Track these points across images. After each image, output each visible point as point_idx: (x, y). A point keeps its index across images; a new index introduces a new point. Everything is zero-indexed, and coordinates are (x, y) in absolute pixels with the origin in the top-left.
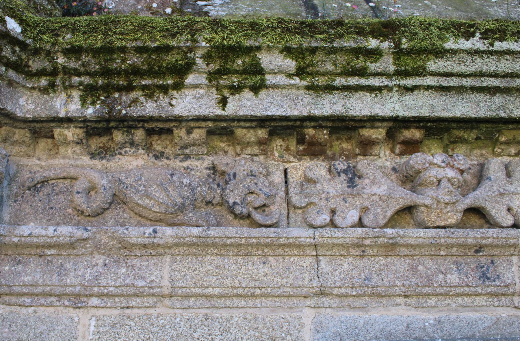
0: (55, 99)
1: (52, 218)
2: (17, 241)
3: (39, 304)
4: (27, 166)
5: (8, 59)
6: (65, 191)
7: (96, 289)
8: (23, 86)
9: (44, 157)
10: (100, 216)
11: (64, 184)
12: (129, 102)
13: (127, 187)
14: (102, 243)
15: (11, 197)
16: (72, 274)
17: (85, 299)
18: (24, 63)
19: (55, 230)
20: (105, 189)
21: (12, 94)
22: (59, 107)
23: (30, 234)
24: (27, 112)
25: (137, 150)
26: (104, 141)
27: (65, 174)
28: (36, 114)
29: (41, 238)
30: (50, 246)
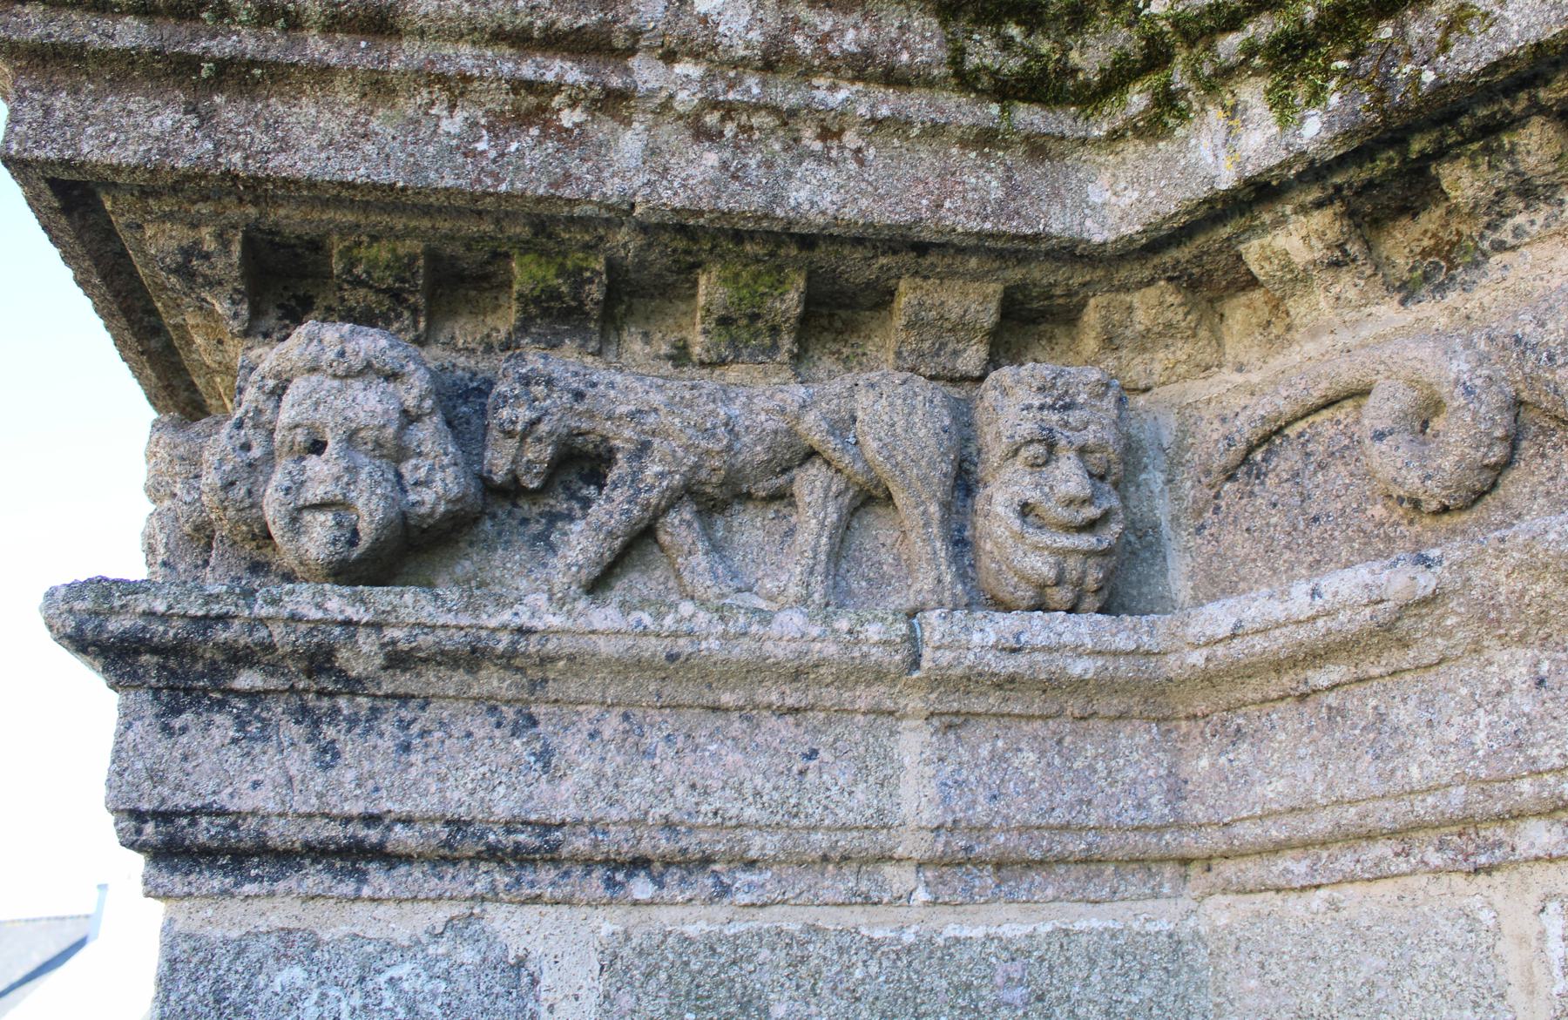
0: (1193, 142)
1: (1323, 553)
2: (1201, 662)
3: (1339, 877)
4: (1209, 402)
5: (994, 74)
6: (1347, 447)
7: (1526, 787)
8: (1084, 141)
9: (1255, 353)
10: (1488, 497)
11: (1338, 422)
12: (1437, 36)
13: (1551, 358)
14: (1502, 599)
15: (1183, 520)
16: (1424, 743)
17: (1501, 833)
18: (1051, 66)
19: (1315, 593)
20: (1469, 391)
21: (1057, 180)
22: (1210, 160)
23: (1236, 627)
24: (1121, 219)
25: (1556, 210)
26: (1432, 227)
27: (1324, 385)
28: (1148, 214)
29: (1277, 632)
30: (1316, 656)
